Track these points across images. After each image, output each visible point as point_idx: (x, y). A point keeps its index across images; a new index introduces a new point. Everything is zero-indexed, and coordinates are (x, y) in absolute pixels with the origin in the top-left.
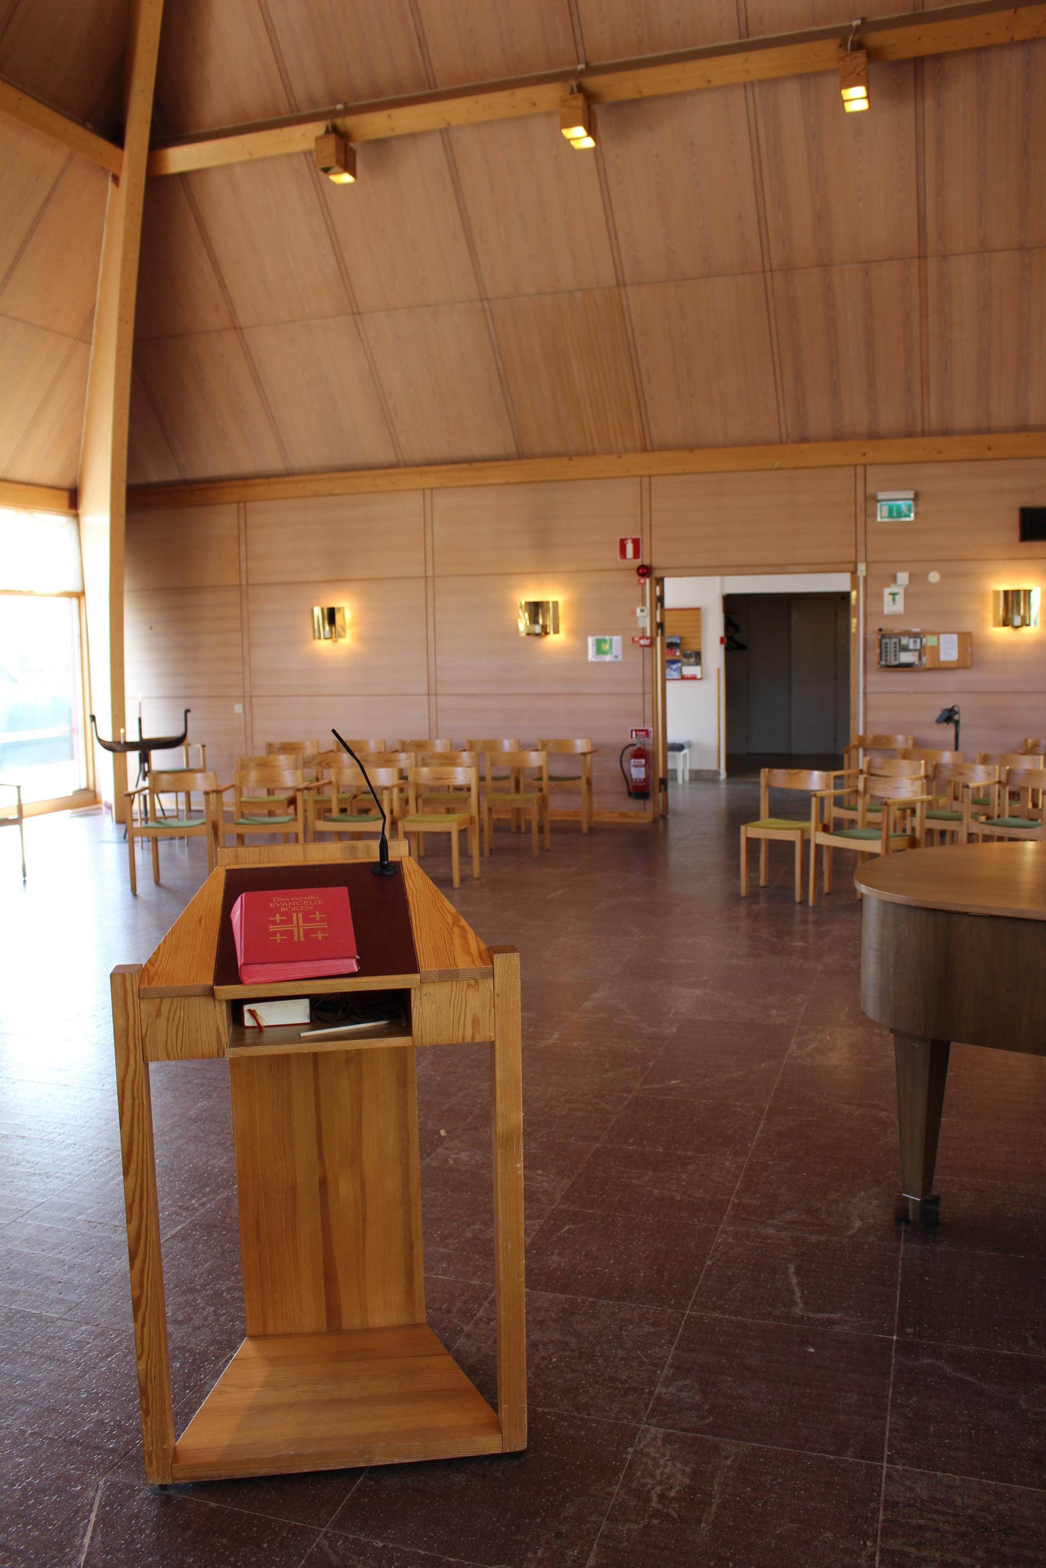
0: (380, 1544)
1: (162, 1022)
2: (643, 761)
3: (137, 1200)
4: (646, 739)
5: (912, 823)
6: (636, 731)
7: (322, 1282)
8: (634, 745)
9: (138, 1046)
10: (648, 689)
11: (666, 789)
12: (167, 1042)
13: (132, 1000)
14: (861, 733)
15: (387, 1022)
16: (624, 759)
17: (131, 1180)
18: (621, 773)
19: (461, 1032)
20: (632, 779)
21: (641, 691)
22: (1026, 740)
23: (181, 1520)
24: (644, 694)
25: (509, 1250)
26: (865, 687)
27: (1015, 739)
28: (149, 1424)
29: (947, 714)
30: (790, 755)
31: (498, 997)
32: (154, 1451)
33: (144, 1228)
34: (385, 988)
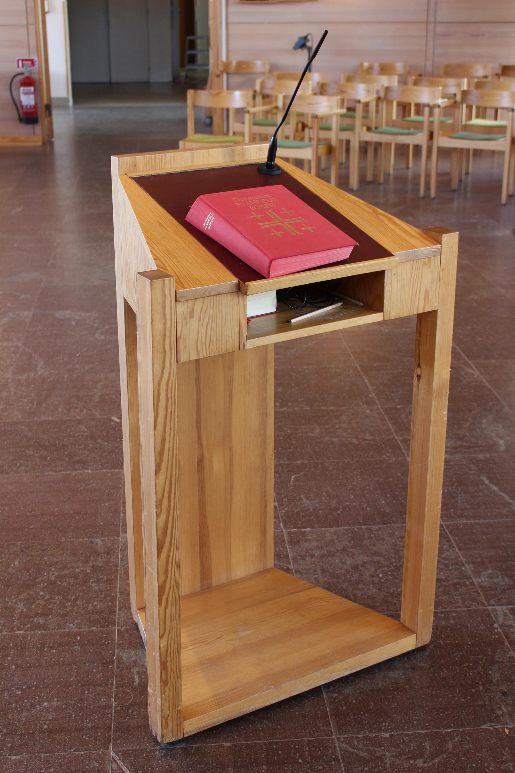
0: (387, 735)
1: (194, 323)
2: (32, 89)
3: (166, 494)
4: (33, 68)
5: (309, 134)
6: (23, 60)
7: (198, 549)
8: (22, 74)
9: (173, 348)
10: (31, 20)
11: (50, 114)
12: (197, 341)
13: (169, 304)
14: (224, 59)
15: (342, 303)
16: (13, 87)
17: (162, 476)
18: (11, 101)
19: (416, 305)
20: (22, 106)
21: (25, 23)
22: (362, 64)
23: (213, 763)
24: (27, 24)
25: (433, 484)
26: (227, 19)
27: (351, 63)
28: (167, 693)
29: (302, 42)
30: (110, 83)
31: (442, 271)
32: (170, 714)
33: (171, 518)
34: (374, 271)
